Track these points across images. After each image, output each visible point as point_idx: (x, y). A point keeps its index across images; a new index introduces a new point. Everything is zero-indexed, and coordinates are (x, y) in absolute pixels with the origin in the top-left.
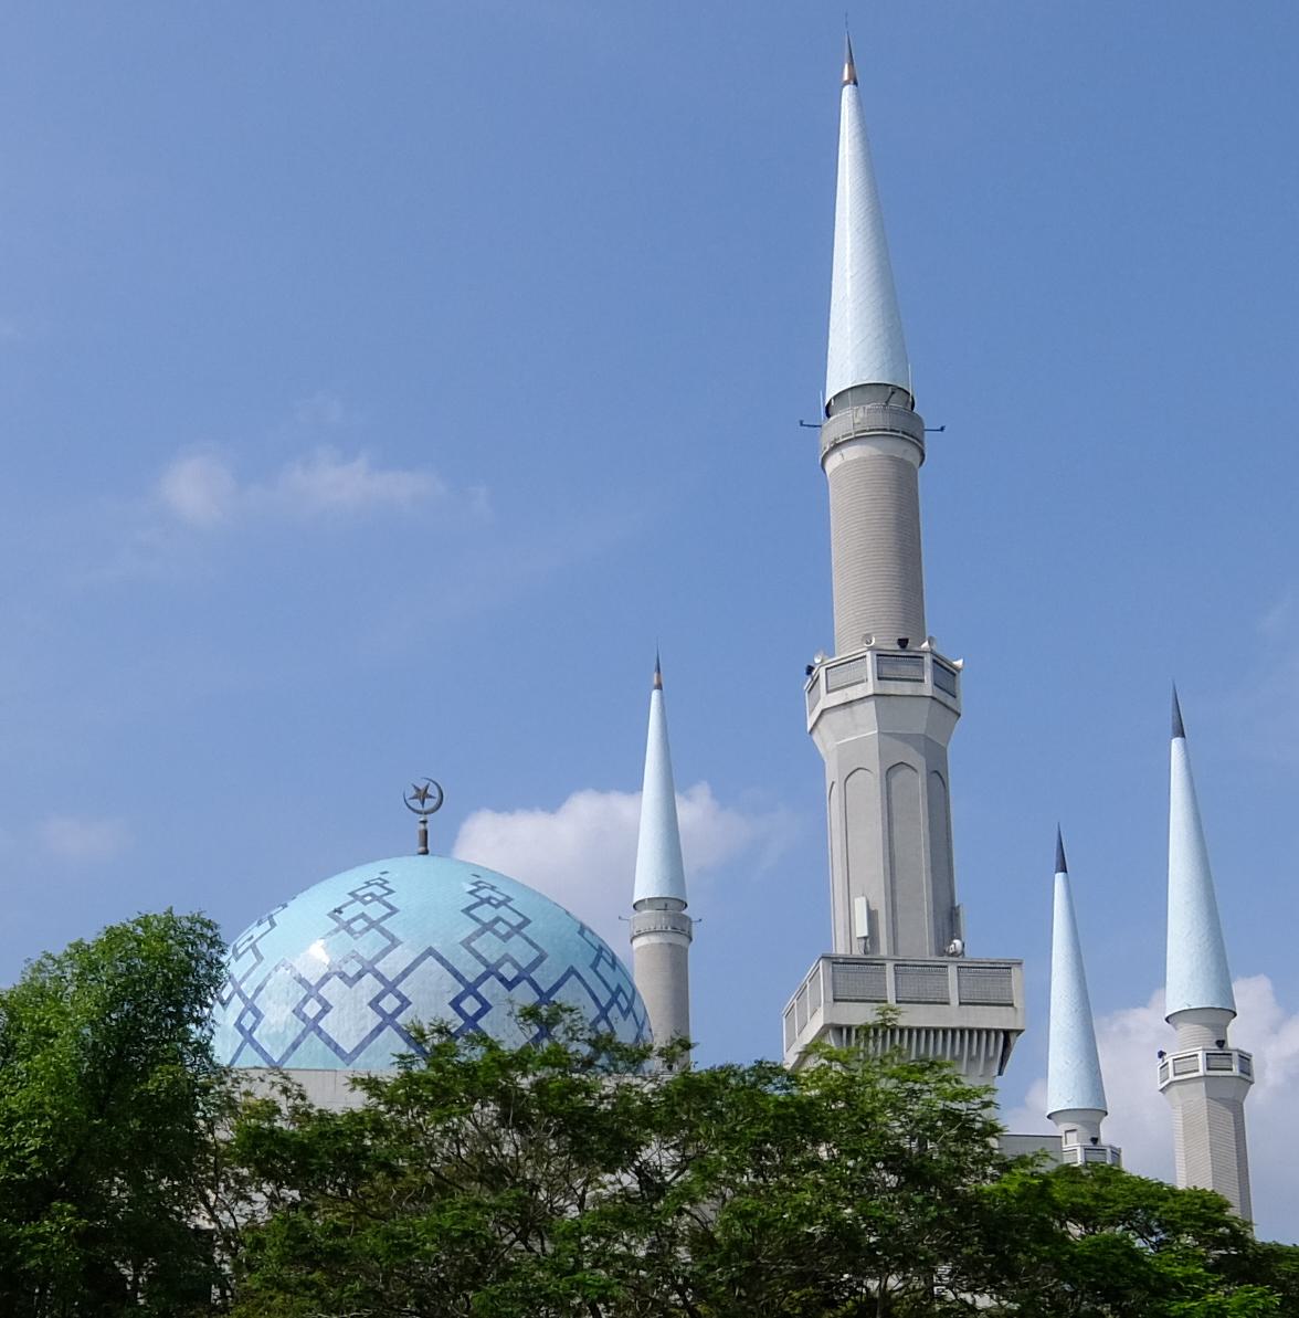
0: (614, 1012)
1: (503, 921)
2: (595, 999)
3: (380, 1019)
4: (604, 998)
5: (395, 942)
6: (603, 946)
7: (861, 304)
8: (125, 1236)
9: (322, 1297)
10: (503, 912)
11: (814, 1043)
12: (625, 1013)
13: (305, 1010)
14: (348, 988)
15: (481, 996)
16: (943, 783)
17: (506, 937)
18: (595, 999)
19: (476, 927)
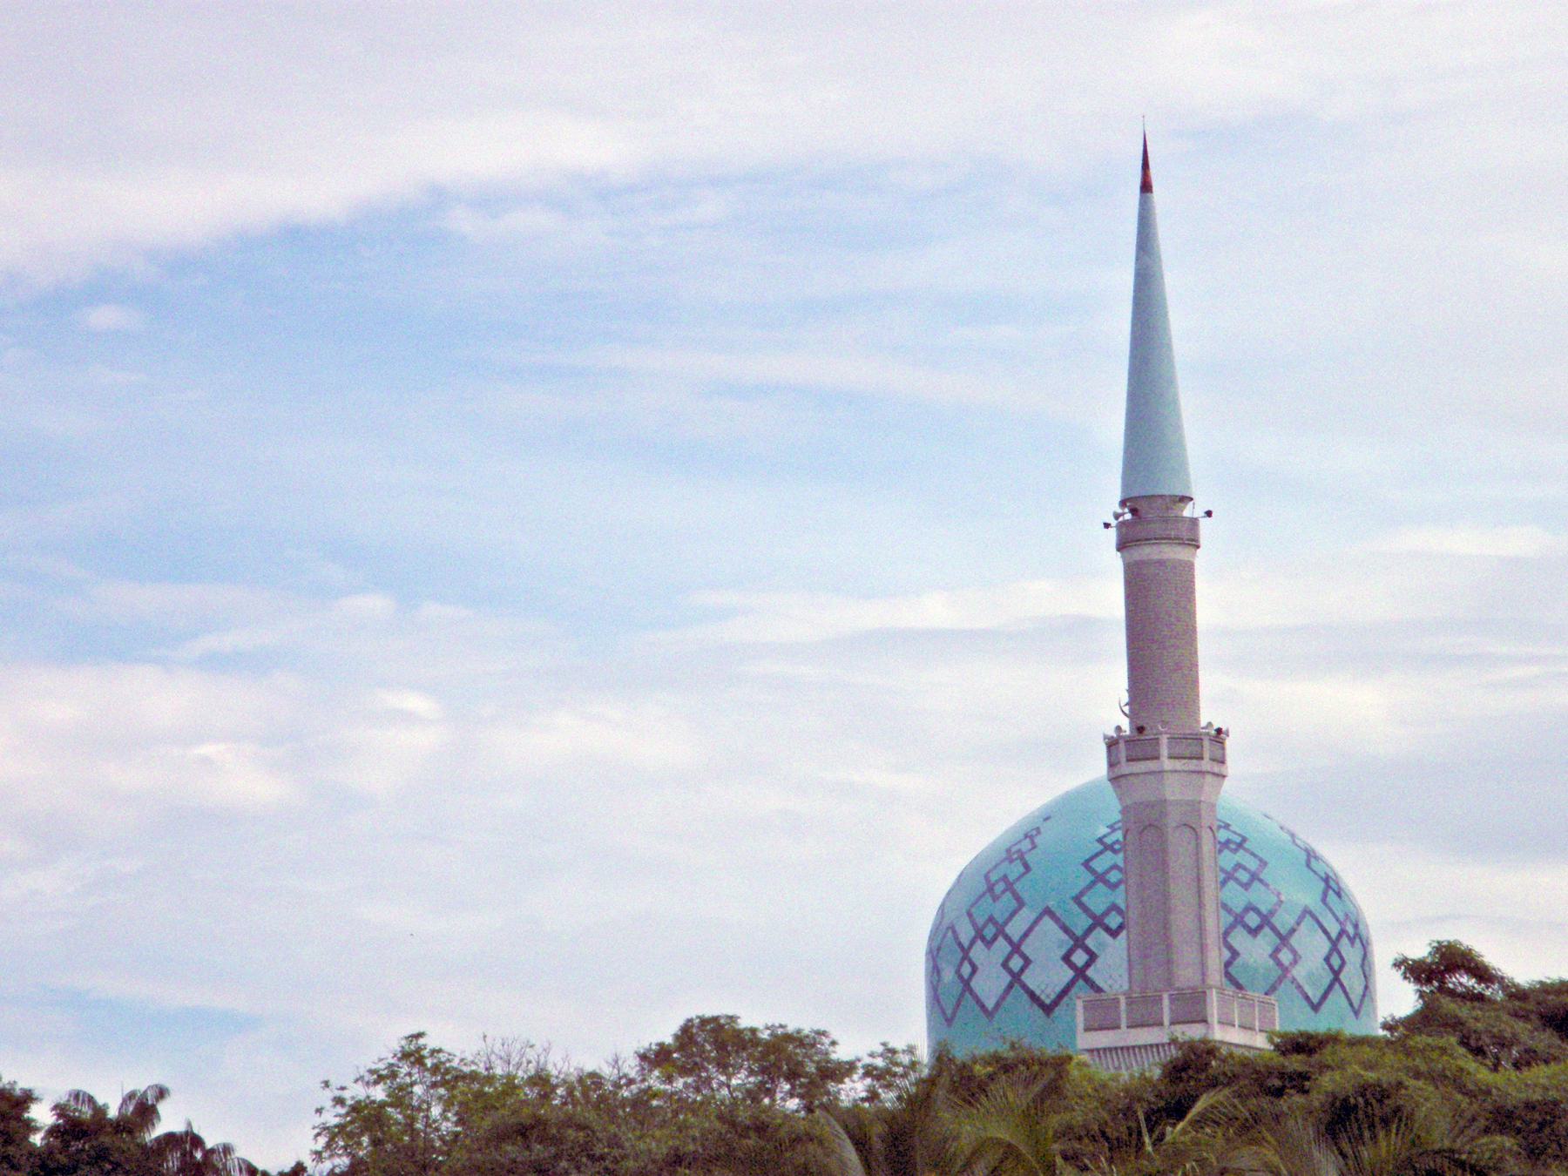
0: (1344, 944)
1: (1024, 874)
2: (1325, 932)
3: (1090, 921)
4: (1334, 930)
5: (1021, 903)
6: (1331, 874)
7: (1176, 647)
8: (1537, 1151)
9: (1152, 1067)
10: (1241, 857)
11: (936, 944)
12: (1352, 941)
13: (1241, 871)
14: (1074, 895)
15: (1276, 929)
16: (943, 911)
17: (1246, 886)
18: (1325, 932)
19: (1090, 878)
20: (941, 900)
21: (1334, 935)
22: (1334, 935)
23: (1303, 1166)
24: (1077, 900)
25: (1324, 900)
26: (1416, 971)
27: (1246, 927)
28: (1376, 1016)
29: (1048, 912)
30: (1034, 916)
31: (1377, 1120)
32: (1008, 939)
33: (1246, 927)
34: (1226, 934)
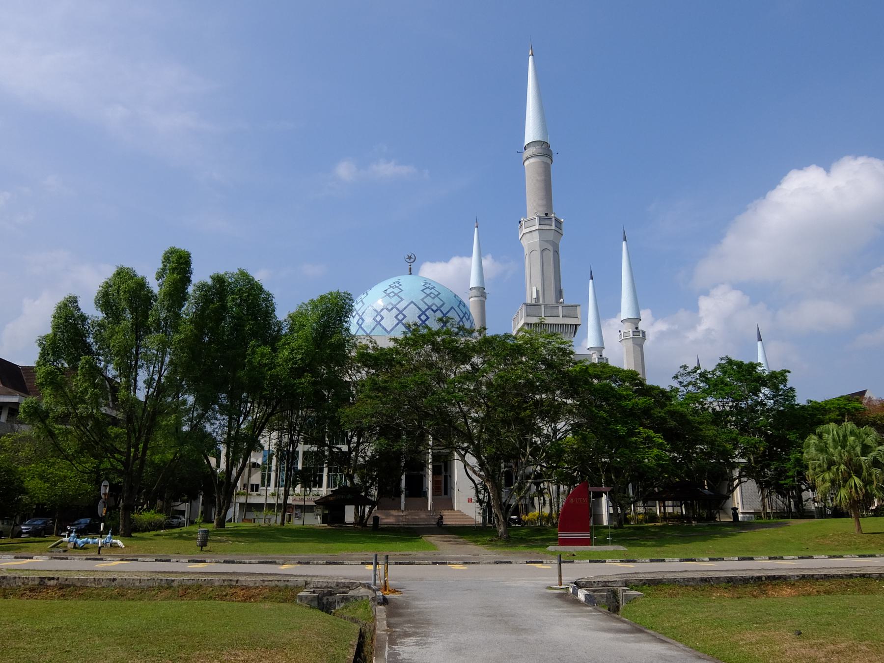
2: (459, 316)
10: (433, 291)
12: (467, 320)
17: (434, 298)
18: (459, 316)
20: (560, 255)
21: (461, 317)
22: (461, 317)
23: (503, 450)
24: (422, 300)
25: (458, 306)
26: (158, 281)
27: (398, 315)
28: (856, 476)
29: (412, 302)
30: (407, 303)
31: (846, 611)
32: (397, 309)
33: (398, 315)
34: (860, 529)
